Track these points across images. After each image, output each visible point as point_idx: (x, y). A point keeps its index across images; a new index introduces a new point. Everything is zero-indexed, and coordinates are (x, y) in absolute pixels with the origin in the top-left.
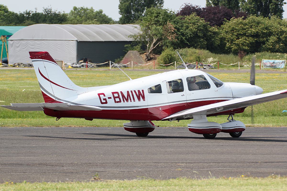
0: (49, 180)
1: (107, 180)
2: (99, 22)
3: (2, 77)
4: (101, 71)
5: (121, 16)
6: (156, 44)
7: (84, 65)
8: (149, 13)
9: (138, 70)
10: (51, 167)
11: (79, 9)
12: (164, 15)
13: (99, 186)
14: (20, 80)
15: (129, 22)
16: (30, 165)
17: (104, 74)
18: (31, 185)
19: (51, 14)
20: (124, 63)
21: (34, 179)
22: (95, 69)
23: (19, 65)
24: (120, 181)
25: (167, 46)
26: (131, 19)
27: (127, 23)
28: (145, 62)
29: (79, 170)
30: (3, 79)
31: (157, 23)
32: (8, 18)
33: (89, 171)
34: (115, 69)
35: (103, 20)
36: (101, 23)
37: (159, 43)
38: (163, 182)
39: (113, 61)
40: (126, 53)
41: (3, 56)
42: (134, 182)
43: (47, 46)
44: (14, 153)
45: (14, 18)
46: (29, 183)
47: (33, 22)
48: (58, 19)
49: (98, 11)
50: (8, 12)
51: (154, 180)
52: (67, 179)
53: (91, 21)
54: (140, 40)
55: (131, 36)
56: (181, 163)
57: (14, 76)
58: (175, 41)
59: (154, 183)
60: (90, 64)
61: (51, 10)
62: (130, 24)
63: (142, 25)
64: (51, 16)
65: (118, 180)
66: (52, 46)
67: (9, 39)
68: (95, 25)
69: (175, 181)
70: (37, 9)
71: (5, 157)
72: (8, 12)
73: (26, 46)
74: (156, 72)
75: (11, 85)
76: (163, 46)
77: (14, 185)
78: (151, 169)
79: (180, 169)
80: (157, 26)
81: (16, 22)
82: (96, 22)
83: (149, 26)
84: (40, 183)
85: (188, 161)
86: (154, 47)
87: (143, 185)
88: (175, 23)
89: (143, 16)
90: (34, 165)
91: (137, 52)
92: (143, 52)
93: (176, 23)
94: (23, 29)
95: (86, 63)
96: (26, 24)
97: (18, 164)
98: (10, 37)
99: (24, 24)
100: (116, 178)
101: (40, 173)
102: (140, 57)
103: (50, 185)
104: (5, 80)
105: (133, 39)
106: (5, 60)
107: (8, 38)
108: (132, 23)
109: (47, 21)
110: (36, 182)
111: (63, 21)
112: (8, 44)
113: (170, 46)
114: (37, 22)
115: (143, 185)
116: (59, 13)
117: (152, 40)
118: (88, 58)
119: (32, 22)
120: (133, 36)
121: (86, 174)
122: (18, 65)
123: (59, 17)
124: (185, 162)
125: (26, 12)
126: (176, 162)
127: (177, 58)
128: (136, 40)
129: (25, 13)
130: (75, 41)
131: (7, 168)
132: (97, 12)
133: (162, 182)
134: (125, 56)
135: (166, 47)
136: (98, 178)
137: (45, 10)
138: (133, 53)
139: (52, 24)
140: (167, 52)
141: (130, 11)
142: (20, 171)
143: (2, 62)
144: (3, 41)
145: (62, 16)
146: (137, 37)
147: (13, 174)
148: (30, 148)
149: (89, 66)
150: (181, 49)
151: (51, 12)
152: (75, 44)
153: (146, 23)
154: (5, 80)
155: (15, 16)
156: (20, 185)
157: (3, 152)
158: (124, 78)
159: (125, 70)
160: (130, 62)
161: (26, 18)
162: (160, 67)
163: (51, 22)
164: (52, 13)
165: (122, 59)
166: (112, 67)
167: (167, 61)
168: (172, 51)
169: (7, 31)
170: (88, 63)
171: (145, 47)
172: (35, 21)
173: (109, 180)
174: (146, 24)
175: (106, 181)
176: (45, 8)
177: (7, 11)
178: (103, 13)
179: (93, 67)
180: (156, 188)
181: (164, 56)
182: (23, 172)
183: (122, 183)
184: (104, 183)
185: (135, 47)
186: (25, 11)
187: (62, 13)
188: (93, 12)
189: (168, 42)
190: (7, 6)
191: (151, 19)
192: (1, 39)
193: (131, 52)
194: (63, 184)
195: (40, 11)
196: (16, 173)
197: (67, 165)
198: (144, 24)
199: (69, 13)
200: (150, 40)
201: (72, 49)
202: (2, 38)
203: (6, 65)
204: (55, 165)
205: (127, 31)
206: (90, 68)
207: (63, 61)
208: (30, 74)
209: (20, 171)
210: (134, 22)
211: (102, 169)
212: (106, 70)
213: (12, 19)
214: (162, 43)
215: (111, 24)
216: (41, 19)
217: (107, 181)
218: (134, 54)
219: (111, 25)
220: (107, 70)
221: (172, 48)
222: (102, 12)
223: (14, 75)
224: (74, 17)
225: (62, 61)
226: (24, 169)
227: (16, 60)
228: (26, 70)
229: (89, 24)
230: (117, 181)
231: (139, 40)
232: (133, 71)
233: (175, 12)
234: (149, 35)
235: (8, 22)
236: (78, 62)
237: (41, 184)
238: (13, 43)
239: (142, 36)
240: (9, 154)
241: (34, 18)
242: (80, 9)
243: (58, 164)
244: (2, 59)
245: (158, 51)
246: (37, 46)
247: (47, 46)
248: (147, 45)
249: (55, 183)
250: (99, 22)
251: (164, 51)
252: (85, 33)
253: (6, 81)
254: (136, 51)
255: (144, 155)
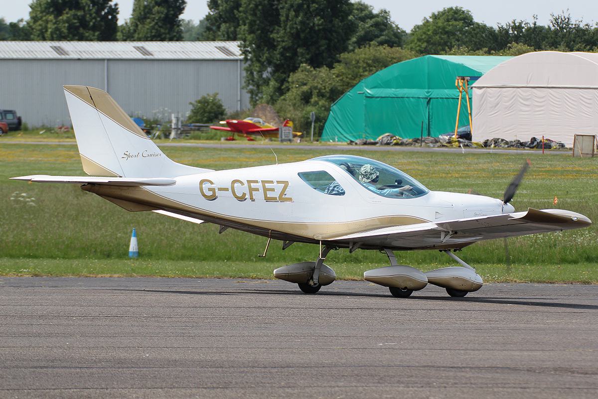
10: (582, 375)
14: (499, 177)
16: (535, 372)
19: (568, 29)
32: (473, 37)
41: (462, 124)
43: (559, 101)
44: (496, 343)
50: (473, 24)
66: (570, 101)
67: (473, 85)
71: (476, 352)
75: (478, 187)
81: (490, 46)
90: (543, 371)
94: (504, 62)
97: (508, 368)
98: (477, 81)
101: (560, 389)
104: (465, 178)
112: (471, 95)
114: (538, 48)
116: (587, 27)
119: (526, 47)
123: (586, 37)
125: (512, 24)
131: (483, 376)
137: (556, 20)
139: (572, 51)
142: (514, 384)
148: (532, 332)
151: (568, 24)
154: (465, 178)
157: (471, 341)
161: (513, 37)
163: (569, 48)
164: (570, 26)
176: (556, 15)
177: (471, 21)
182: (520, 386)
186: (511, 23)
187: (593, 28)
190: (469, 11)
195: (545, 22)
196: (505, 389)
202: (458, 82)
203: (467, 142)
209: (514, 384)
213: (481, 41)
223: (485, 166)
226: (521, 379)
238: (483, 95)
240: (485, 345)
241: (530, 38)
244: (459, 130)
247: (559, 101)
253: (468, 180)
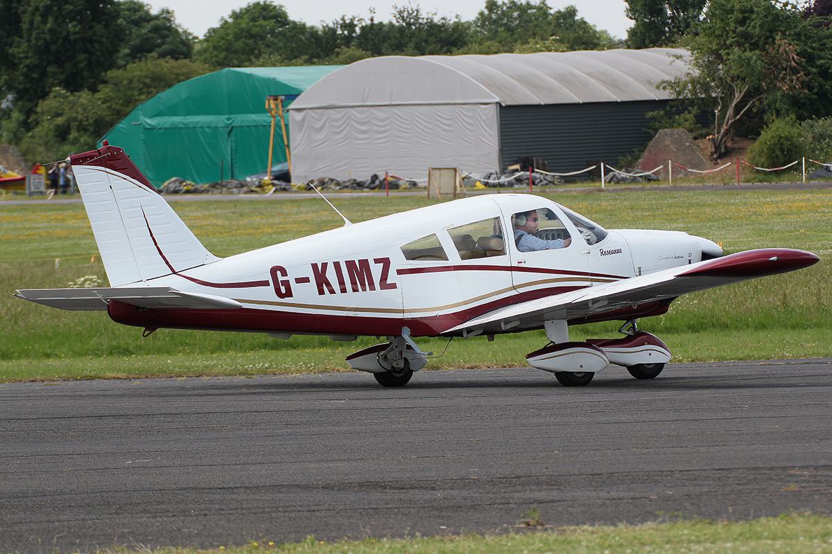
0: (386, 531)
1: (565, 527)
2: (566, 45)
3: (273, 224)
4: (574, 193)
5: (632, 23)
6: (744, 108)
7: (521, 178)
8: (717, 12)
9: (688, 189)
11: (505, 8)
12: (766, 16)
13: (539, 545)
15: (657, 42)
16: (332, 489)
17: (586, 203)
18: (328, 550)
20: (645, 169)
21: (340, 528)
22: (556, 190)
23: (324, 186)
24: (605, 528)
25: (778, 112)
26: (664, 32)
27: (652, 45)
28: (710, 162)
29: (482, 497)
30: (274, 229)
31: (746, 40)
33: (511, 501)
34: (618, 187)
35: (579, 38)
36: (572, 48)
37: (751, 102)
38: (737, 528)
39: (610, 162)
40: (651, 137)
42: (648, 529)
45: (306, 42)
46: (322, 542)
47: (364, 52)
48: (441, 41)
49: (563, 10)
50: (288, 24)
51: (710, 523)
52: (442, 527)
53: (541, 42)
54: (692, 95)
55: (664, 85)
56: (800, 468)
57: (308, 218)
58: (802, 96)
59: (709, 530)
60: (542, 174)
61: (417, 14)
62: (660, 46)
63: (699, 49)
64: (417, 31)
65: (596, 526)
68: (553, 54)
69: (775, 524)
70: (374, 13)
72: (288, 24)
73: (344, 126)
74: (745, 190)
76: (764, 112)
77: (276, 549)
78: (705, 489)
79: (793, 487)
80: (745, 51)
81: (313, 53)
82: (556, 45)
83: (720, 52)
84: (356, 542)
85: (823, 462)
86: (738, 117)
87: (675, 539)
88: (799, 40)
89: (702, 22)
91: (686, 131)
92: (704, 131)
93: (803, 38)
95: (528, 173)
96: (341, 57)
99: (336, 59)
100: (592, 520)
102: (695, 147)
103: (387, 546)
104: (281, 233)
105: (672, 94)
106: (282, 171)
107: (290, 103)
108: (667, 45)
109: (406, 47)
110: (346, 538)
111: (455, 46)
112: (288, 121)
113: (788, 111)
115: (675, 539)
116: (443, 21)
117: (732, 93)
118: (536, 156)
119: (359, 52)
120: (671, 85)
121: (501, 510)
122: (322, 185)
123: (443, 35)
124: (812, 466)
125: (341, 22)
126: (786, 464)
127: (807, 147)
128: (681, 97)
129: (339, 26)
130: (494, 106)
132: (559, 15)
133: (734, 527)
134: (648, 145)
135: (775, 115)
136: (537, 521)
138: (671, 135)
139: (423, 54)
140: (778, 128)
141: (660, 7)
143: (271, 177)
144: (273, 112)
145: (453, 30)
146: (685, 86)
147: (276, 518)
149: (537, 181)
150: (819, 119)
151: (417, 18)
152: (492, 114)
153: (711, 43)
154: (281, 233)
155: (308, 36)
156: (295, 548)
158: (644, 214)
159: (649, 189)
160: (662, 164)
161: (341, 39)
162: (757, 175)
164: (420, 21)
165: (639, 154)
166: (610, 182)
167: (777, 157)
168: (793, 126)
169: (286, 82)
170: (533, 171)
171: (710, 117)
172: (369, 48)
173: (573, 528)
174: (710, 46)
175: (561, 530)
176: (400, 7)
177: (286, 20)
178: (576, 18)
179: (550, 182)
180: (712, 545)
181: (768, 143)
183: (608, 535)
184: (553, 536)
185: (677, 117)
187: (452, 22)
188: (546, 14)
189: (779, 97)
191: (724, 29)
192: (267, 107)
193: (666, 134)
194: (428, 543)
195: (385, 16)
197: (446, 483)
198: (703, 45)
199: (474, 21)
200: (723, 93)
201: (485, 130)
202: (269, 104)
203: (283, 184)
204: (409, 486)
205: (615, 70)
206: (542, 185)
207: (457, 169)
208: (358, 212)
210: (674, 42)
211: (554, 494)
212: (590, 192)
214: (761, 103)
215: (603, 49)
216: (389, 41)
217: (565, 530)
218: (675, 139)
219: (604, 51)
220: (592, 192)
221: (793, 116)
222: (575, 15)
223: (309, 216)
224: (490, 30)
225: (455, 170)
226: (311, 499)
227: (316, 169)
228: (345, 200)
229: (535, 52)
230: (595, 529)
231: (689, 96)
232: (674, 192)
233: (799, 7)
234: (721, 79)
235: (288, 53)
236: (503, 171)
237: (360, 544)
238: (303, 120)
239: (700, 83)
242: (508, 8)
243: (419, 481)
245: (748, 127)
246: (377, 125)
248: (716, 111)
249: (403, 541)
250: (564, 43)
251: (768, 127)
252: (522, 79)
253: (285, 236)
254: (681, 129)
255: (686, 447)
